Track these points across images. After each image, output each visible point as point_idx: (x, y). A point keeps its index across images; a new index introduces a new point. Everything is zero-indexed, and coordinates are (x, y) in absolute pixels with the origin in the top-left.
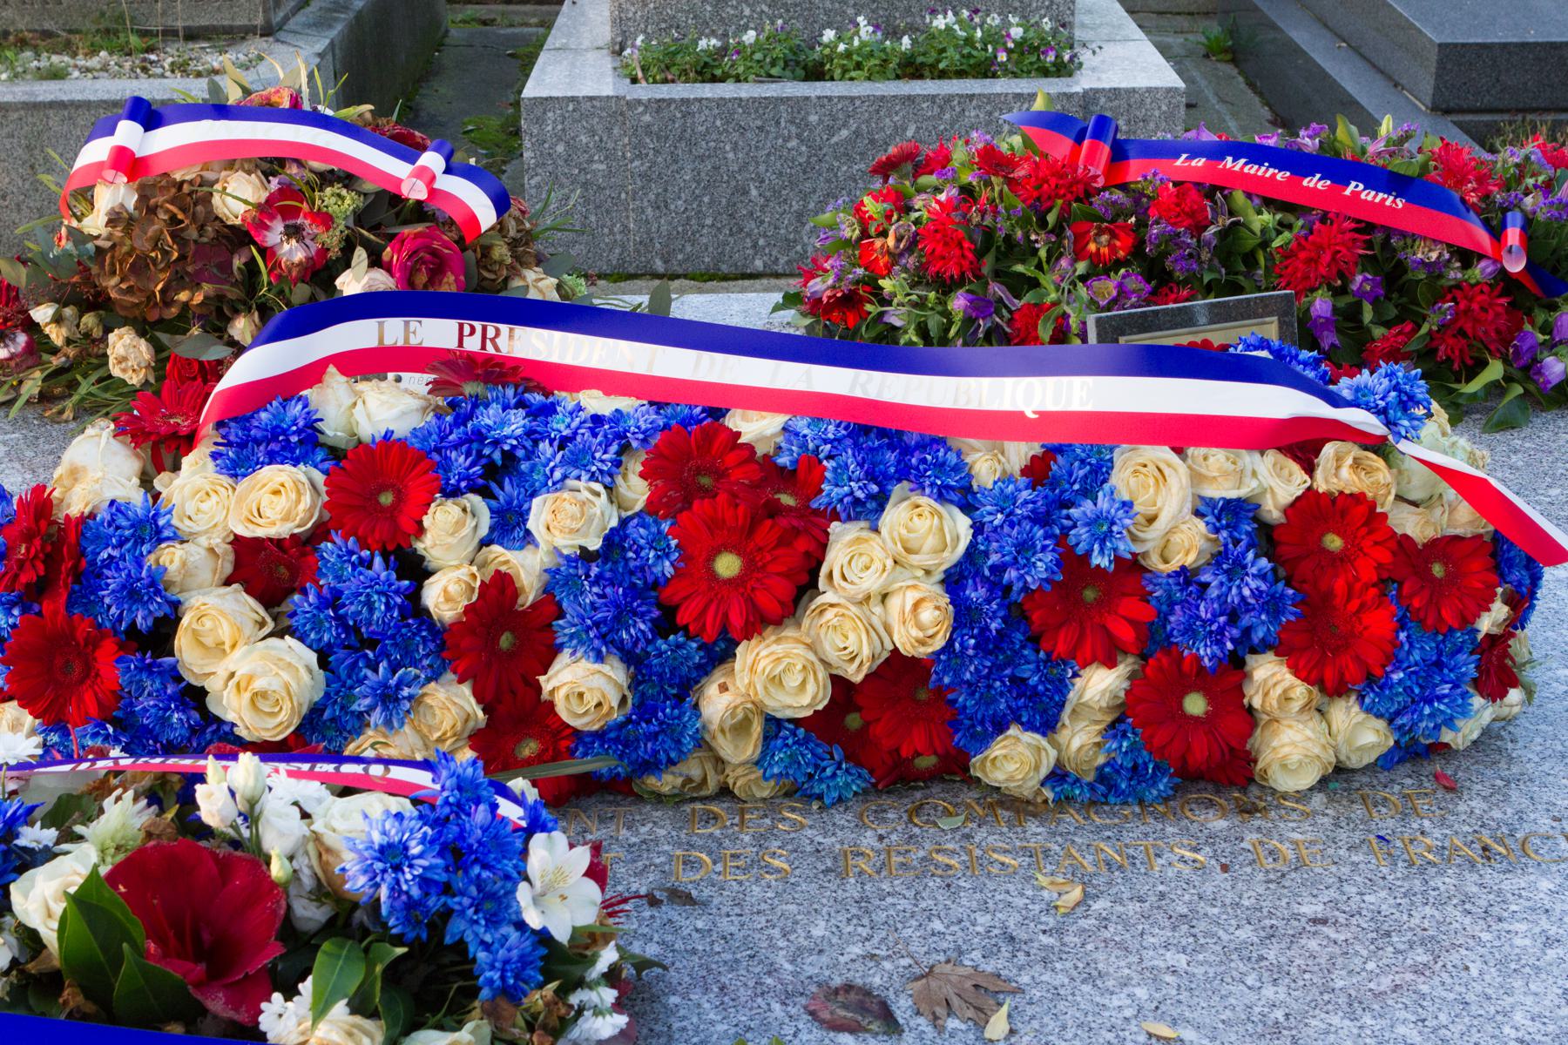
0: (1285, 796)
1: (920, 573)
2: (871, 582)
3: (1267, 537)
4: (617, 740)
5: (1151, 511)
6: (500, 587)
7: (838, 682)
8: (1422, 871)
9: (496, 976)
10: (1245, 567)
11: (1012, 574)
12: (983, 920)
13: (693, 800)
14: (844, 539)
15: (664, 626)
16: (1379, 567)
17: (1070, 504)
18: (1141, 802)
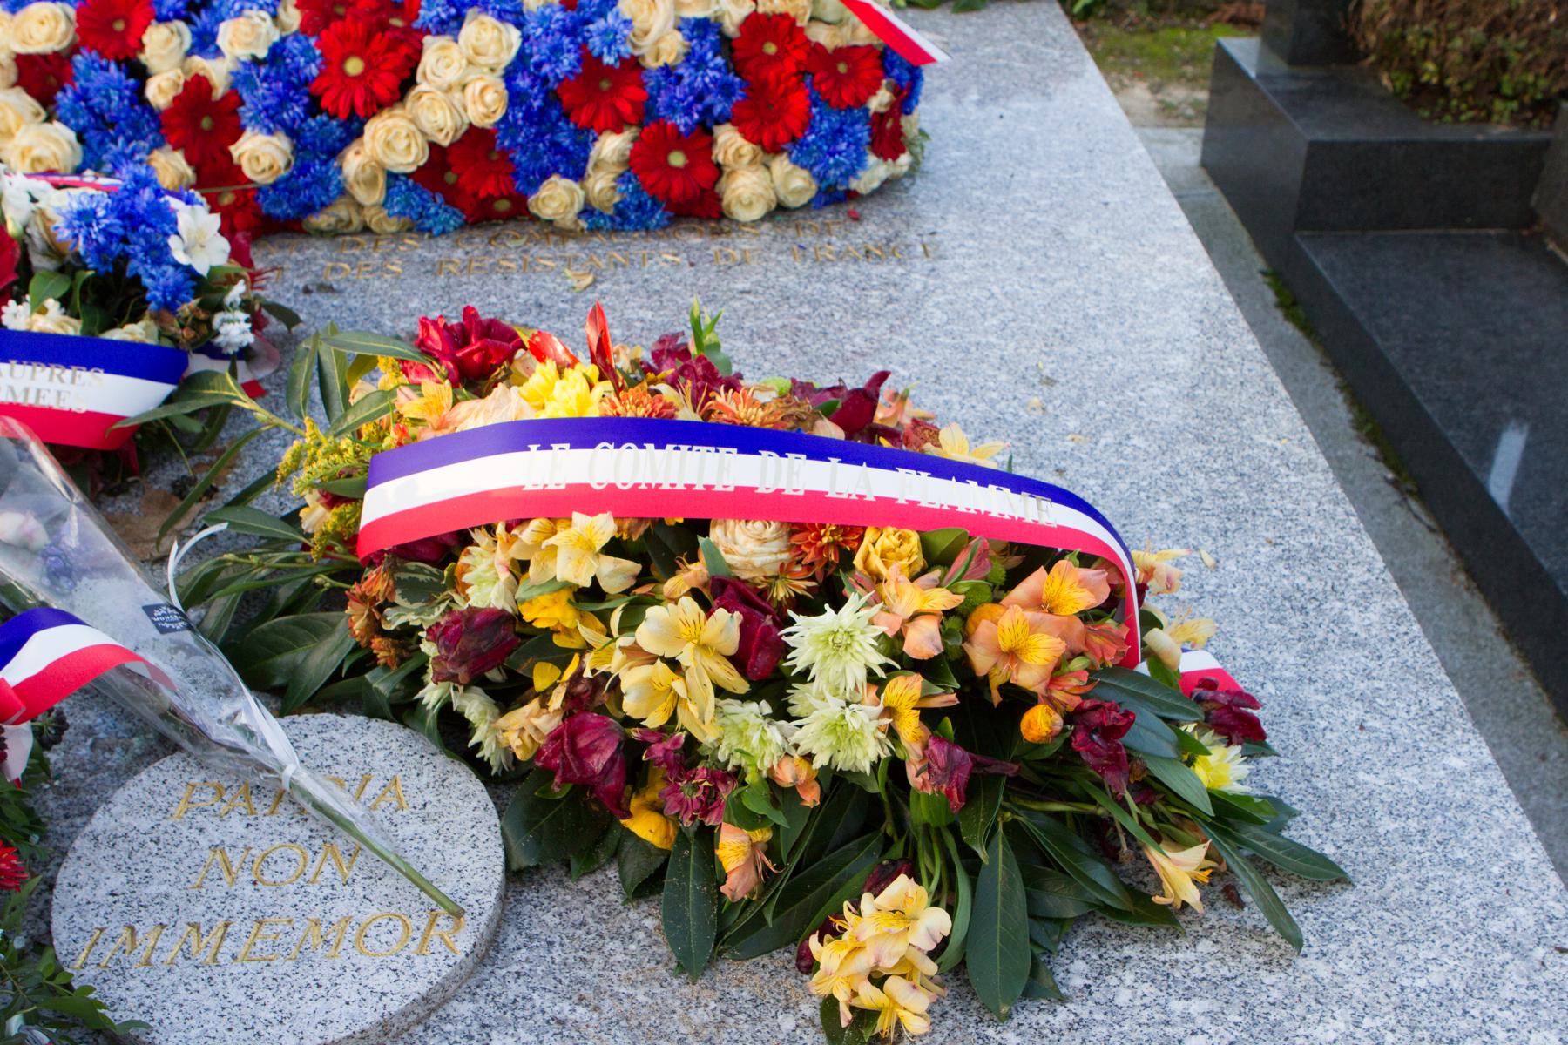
0: (745, 224)
1: (486, 70)
2: (451, 76)
3: (725, 44)
4: (285, 189)
5: (646, 26)
6: (197, 87)
7: (433, 146)
8: (822, 264)
9: (158, 294)
10: (706, 63)
11: (546, 68)
12: (524, 296)
13: (344, 234)
14: (433, 47)
15: (313, 109)
16: (798, 63)
17: (589, 22)
18: (647, 229)
